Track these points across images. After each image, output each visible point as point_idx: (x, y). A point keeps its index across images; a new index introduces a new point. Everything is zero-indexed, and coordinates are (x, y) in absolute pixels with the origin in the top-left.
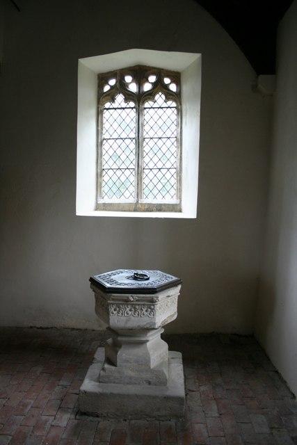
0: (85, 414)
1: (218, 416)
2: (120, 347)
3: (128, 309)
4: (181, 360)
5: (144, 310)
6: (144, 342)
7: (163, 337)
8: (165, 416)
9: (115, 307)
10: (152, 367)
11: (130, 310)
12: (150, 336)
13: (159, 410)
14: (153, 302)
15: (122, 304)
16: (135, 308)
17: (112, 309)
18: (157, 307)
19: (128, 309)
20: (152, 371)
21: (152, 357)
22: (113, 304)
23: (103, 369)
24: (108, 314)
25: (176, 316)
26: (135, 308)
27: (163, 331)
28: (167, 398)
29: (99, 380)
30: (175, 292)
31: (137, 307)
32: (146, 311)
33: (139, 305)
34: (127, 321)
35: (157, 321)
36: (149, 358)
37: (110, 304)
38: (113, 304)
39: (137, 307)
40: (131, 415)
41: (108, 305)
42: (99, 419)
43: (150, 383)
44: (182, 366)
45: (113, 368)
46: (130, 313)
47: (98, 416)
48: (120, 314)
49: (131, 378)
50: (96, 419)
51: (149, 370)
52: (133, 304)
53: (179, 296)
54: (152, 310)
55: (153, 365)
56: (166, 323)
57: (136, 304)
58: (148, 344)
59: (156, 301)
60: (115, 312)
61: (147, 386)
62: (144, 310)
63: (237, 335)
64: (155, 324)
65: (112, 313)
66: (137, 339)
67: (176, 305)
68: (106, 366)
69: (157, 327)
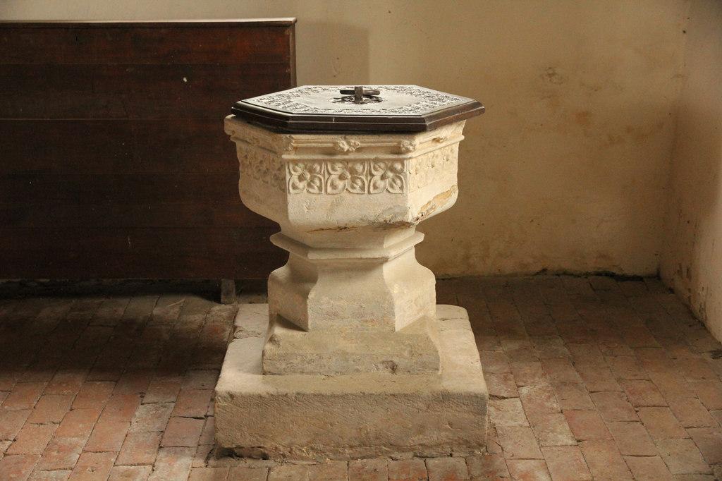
0: (230, 453)
1: (574, 442)
2: (313, 280)
3: (335, 175)
4: (468, 323)
5: (378, 174)
6: (374, 265)
7: (423, 254)
8: (439, 445)
9: (300, 169)
10: (398, 327)
11: (341, 177)
12: (390, 248)
13: (421, 429)
14: (399, 153)
15: (320, 162)
16: (353, 171)
17: (292, 177)
18: (411, 166)
19: (335, 175)
20: (399, 338)
21: (398, 303)
22: (296, 162)
23: (272, 340)
24: (283, 191)
25: (455, 196)
26: (353, 171)
27: (420, 238)
28: (445, 398)
29: (263, 370)
30: (453, 135)
31: (359, 168)
32: (383, 178)
33: (362, 161)
34: (335, 205)
35: (410, 203)
36: (391, 305)
37: (288, 161)
38: (296, 162)
39: (359, 168)
40: (351, 447)
41: (282, 168)
42: (269, 463)
43: (394, 368)
44: (471, 333)
45: (298, 335)
46: (340, 184)
47: (265, 457)
48: (316, 190)
49: (344, 355)
50: (262, 463)
51: (390, 335)
52: (348, 161)
53: (462, 144)
54: (398, 174)
55: (401, 321)
56: (433, 213)
57: (355, 161)
58: (387, 269)
59: (408, 151)
60: (301, 185)
61: (387, 373)
62: (378, 174)
63: (612, 275)
64: (405, 212)
65: (295, 187)
66: (364, 255)
67: (455, 169)
68: (279, 331)
69: (410, 219)
